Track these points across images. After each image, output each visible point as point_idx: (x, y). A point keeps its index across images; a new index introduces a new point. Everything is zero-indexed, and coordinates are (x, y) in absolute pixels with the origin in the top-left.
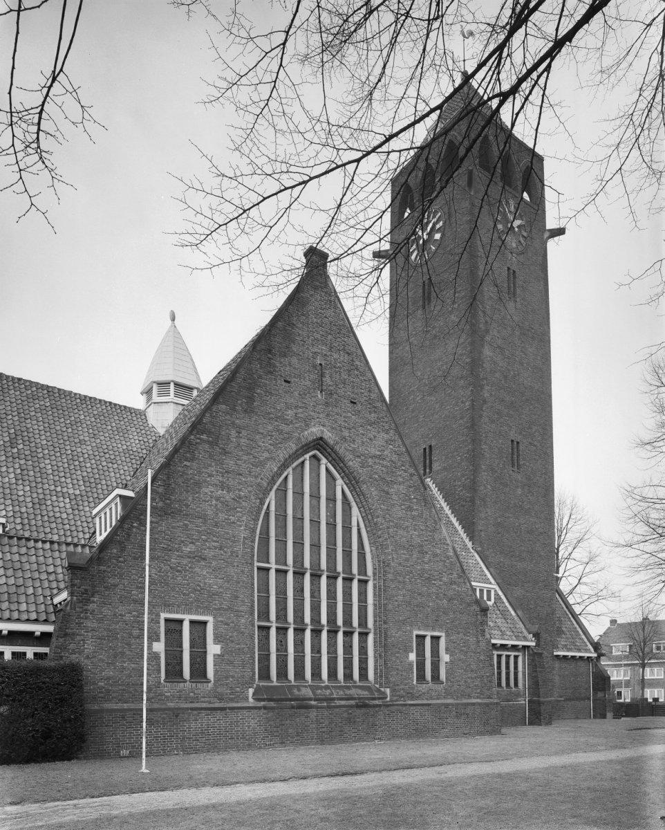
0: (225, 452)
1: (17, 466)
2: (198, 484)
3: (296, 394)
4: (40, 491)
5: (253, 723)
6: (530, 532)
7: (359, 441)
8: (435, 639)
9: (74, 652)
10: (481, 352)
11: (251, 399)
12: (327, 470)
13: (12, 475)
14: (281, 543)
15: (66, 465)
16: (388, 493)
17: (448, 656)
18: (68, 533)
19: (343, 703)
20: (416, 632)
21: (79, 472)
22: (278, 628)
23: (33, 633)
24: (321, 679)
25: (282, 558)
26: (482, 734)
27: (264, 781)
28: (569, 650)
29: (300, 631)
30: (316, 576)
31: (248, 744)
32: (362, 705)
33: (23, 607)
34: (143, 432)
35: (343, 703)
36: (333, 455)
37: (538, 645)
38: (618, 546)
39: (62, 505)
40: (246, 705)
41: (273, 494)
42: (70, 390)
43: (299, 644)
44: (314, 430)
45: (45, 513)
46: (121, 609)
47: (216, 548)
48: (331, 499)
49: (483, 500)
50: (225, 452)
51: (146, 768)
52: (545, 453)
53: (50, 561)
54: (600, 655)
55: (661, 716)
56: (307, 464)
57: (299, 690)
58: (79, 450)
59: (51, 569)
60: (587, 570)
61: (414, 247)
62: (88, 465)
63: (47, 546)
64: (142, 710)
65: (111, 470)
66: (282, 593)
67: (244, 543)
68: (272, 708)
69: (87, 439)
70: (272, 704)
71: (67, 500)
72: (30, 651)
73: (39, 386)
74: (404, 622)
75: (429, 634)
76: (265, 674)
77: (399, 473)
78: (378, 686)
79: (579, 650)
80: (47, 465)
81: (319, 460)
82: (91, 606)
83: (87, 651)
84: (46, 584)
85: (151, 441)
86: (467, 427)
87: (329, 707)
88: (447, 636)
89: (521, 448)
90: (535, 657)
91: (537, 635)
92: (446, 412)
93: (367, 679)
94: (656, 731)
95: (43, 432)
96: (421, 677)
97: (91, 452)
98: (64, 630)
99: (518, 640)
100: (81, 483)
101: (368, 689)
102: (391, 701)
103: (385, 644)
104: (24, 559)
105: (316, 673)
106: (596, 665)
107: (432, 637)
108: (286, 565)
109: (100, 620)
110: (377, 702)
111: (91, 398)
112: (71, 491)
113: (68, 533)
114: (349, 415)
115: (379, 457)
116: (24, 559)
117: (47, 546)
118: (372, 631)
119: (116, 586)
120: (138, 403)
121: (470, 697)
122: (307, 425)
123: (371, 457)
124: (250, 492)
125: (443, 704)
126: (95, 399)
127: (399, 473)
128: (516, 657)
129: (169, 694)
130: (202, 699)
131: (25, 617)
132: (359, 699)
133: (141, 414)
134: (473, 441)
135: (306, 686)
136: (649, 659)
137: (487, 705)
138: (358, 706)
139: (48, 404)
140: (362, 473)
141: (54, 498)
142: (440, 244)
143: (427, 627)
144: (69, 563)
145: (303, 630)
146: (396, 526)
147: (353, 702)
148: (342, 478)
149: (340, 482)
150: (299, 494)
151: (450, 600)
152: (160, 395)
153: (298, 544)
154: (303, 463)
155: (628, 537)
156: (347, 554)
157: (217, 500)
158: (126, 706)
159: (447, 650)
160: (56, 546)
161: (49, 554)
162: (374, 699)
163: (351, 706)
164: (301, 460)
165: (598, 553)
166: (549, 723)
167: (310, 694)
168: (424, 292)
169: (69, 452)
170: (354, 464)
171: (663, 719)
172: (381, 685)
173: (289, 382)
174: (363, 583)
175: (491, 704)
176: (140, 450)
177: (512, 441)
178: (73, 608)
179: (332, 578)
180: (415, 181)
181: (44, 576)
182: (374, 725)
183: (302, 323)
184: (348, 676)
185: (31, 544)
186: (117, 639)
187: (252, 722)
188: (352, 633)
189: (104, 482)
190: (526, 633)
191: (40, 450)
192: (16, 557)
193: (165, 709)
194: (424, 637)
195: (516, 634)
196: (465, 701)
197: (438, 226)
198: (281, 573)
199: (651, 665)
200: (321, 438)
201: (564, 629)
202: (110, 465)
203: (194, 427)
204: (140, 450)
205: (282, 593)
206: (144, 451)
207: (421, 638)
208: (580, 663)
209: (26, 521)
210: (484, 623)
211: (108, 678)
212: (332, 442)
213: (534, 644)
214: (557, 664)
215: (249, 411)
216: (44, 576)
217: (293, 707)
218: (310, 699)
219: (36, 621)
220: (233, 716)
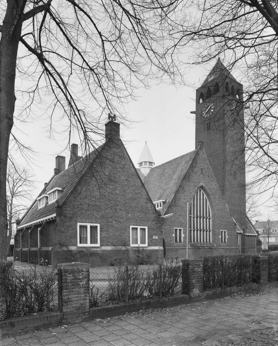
0: (185, 191)
2: (180, 199)
8: (225, 232)
10: (226, 146)
11: (189, 179)
20: (221, 231)
25: (194, 215)
28: (250, 233)
29: (197, 231)
37: (244, 232)
43: (197, 234)
46: (168, 227)
48: (203, 199)
49: (226, 190)
50: (185, 191)
54: (259, 235)
66: (194, 222)
75: (224, 231)
79: (252, 233)
82: (163, 227)
86: (222, 169)
88: (227, 231)
90: (243, 236)
91: (243, 230)
96: (176, 241)
101: (211, 244)
105: (200, 241)
107: (179, 229)
110: (213, 248)
140: (210, 193)
143: (223, 229)
144: (57, 205)
146: (217, 205)
147: (208, 248)
149: (205, 195)
163: (208, 248)
168: (207, 126)
170: (208, 191)
172: (213, 243)
174: (209, 219)
180: (205, 91)
184: (207, 241)
190: (240, 229)
194: (177, 229)
196: (231, 247)
205: (194, 222)
207: (222, 232)
208: (253, 237)
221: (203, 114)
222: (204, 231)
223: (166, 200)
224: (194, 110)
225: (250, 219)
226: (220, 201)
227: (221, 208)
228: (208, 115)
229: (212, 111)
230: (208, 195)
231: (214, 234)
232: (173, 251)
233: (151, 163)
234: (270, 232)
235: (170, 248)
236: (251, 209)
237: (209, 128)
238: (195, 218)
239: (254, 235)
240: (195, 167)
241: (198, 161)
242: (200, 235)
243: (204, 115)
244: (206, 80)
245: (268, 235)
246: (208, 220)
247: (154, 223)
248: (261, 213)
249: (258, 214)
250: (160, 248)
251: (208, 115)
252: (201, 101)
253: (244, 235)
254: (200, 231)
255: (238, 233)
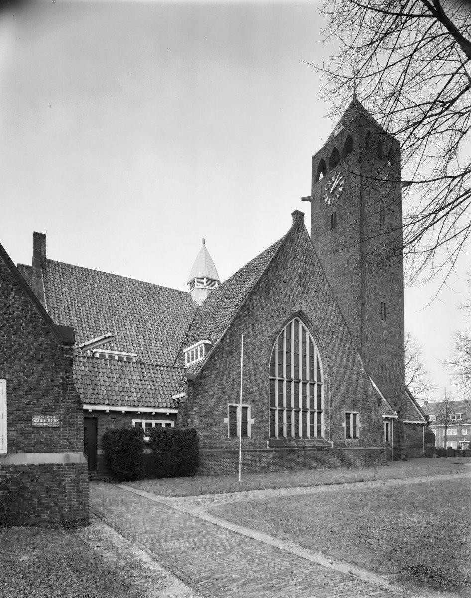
0: (256, 320)
1: (136, 326)
3: (289, 288)
4: (148, 339)
5: (269, 459)
6: (391, 354)
7: (318, 311)
8: (355, 415)
9: (190, 423)
11: (268, 292)
12: (302, 327)
13: (134, 331)
14: (281, 366)
15: (158, 324)
16: (332, 338)
17: (253, 420)
18: (164, 361)
19: (311, 449)
21: (164, 328)
22: (279, 410)
23: (137, 412)
24: (283, 436)
25: (281, 375)
26: (378, 465)
27: (300, 486)
28: (412, 420)
29: (289, 411)
30: (297, 383)
31: (267, 469)
32: (320, 450)
33: (160, 400)
34: (191, 305)
35: (311, 449)
36: (306, 319)
38: (449, 363)
39: (159, 346)
40: (265, 449)
41: (277, 340)
42: (61, 261)
43: (289, 418)
44: (297, 306)
45: (152, 350)
46: (211, 402)
47: (252, 369)
48: (304, 342)
50: (256, 320)
51: (241, 480)
52: (400, 309)
53: (168, 376)
54: (429, 423)
55: (468, 456)
56: (293, 324)
57: (289, 442)
58: (163, 316)
59: (169, 381)
60: (417, 373)
61: (326, 195)
62: (168, 324)
63: (165, 369)
64: (239, 451)
65: (179, 326)
66: (281, 391)
67: (265, 367)
68: (277, 451)
69: (165, 310)
70: (278, 449)
71: (161, 343)
72: (163, 422)
73: (60, 264)
74: (340, 406)
75: (352, 412)
76: (273, 435)
77: (337, 327)
78: (326, 440)
79: (417, 420)
80: (149, 324)
81: (298, 322)
82: (197, 400)
83: (196, 422)
84: (168, 389)
85: (195, 309)
86: (358, 296)
87: (304, 451)
89: (386, 307)
90: (398, 424)
92: (345, 288)
93: (321, 436)
94: (466, 464)
95: (145, 307)
96: (348, 435)
97: (168, 317)
98: (186, 414)
99: (388, 414)
100: (166, 334)
102: (333, 447)
103: (331, 418)
104: (156, 376)
105: (297, 434)
106: (427, 428)
108: (320, 382)
109: (201, 407)
111: (164, 287)
112: (162, 338)
113: (164, 361)
114: (314, 298)
115: (328, 319)
116: (156, 376)
117: (165, 369)
118: (324, 411)
119: (208, 390)
120: (186, 288)
121: (372, 446)
122: (294, 304)
123: (324, 320)
124: (268, 340)
125: (359, 450)
126: (166, 288)
127: (337, 327)
128: (387, 424)
129: (231, 444)
130: (246, 447)
131: (161, 405)
132: (318, 446)
133: (188, 295)
134: (362, 304)
135: (292, 440)
136: (450, 424)
137: (380, 450)
138: (318, 450)
139: (145, 292)
141: (155, 342)
142: (342, 193)
143: (351, 409)
145: (291, 411)
146: (337, 356)
147: (315, 448)
148: (310, 331)
150: (289, 340)
151: (362, 394)
152: (198, 284)
153: (289, 367)
154: (291, 324)
155: (454, 359)
156: (312, 371)
157: (253, 345)
158: (212, 450)
159: (361, 421)
160: (169, 369)
161: (167, 373)
162: (325, 447)
163: (314, 450)
164: (290, 322)
165: (422, 364)
166: (405, 460)
167: (295, 445)
169: (158, 317)
170: (316, 323)
171: (470, 459)
173: (285, 282)
174: (319, 386)
175: (382, 449)
176: (191, 315)
177: (382, 303)
178: (190, 401)
179: (305, 384)
180: (326, 157)
181: (166, 385)
182: (325, 460)
183: (292, 251)
184: (312, 435)
185: (158, 368)
186: (208, 416)
187: (268, 459)
188: (314, 412)
189: (176, 333)
191: (145, 317)
192: (153, 375)
193: (229, 452)
194: (349, 414)
195: (387, 411)
196: (369, 448)
197: (341, 184)
198: (281, 381)
199: (450, 427)
200: (301, 311)
201: (408, 408)
202: (178, 324)
203: (242, 308)
204: (191, 315)
205: (281, 391)
206: (193, 315)
207: (348, 414)
209: (144, 355)
210: (379, 406)
211: (204, 436)
212: (306, 313)
213: (397, 417)
214: (405, 427)
215: (267, 299)
216: (166, 385)
217: (287, 451)
218: (295, 447)
219: (166, 407)
220: (260, 456)
221: (325, 198)
222: (305, 412)
223: (213, 342)
224: (309, 193)
225: (413, 395)
226: (343, 346)
227: (346, 363)
228: (333, 200)
229: (340, 189)
230: (315, 333)
231: (329, 418)
232: (224, 458)
233: (210, 281)
234: (448, 419)
235: (215, 450)
236: (414, 379)
237: (334, 224)
238: (285, 383)
239: (421, 422)
240: (284, 268)
241: (291, 255)
242: (297, 421)
243: (325, 201)
244: (333, 133)
245: (446, 424)
246: (315, 387)
247: (37, 368)
248: (433, 384)
249: (427, 387)
250: (68, 458)
251: (333, 200)
252: (321, 176)
253: (401, 423)
254: (297, 412)
255: (387, 419)
